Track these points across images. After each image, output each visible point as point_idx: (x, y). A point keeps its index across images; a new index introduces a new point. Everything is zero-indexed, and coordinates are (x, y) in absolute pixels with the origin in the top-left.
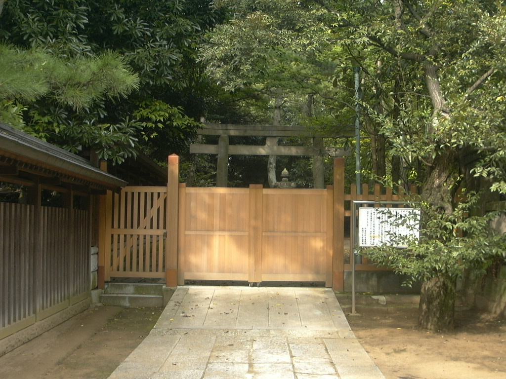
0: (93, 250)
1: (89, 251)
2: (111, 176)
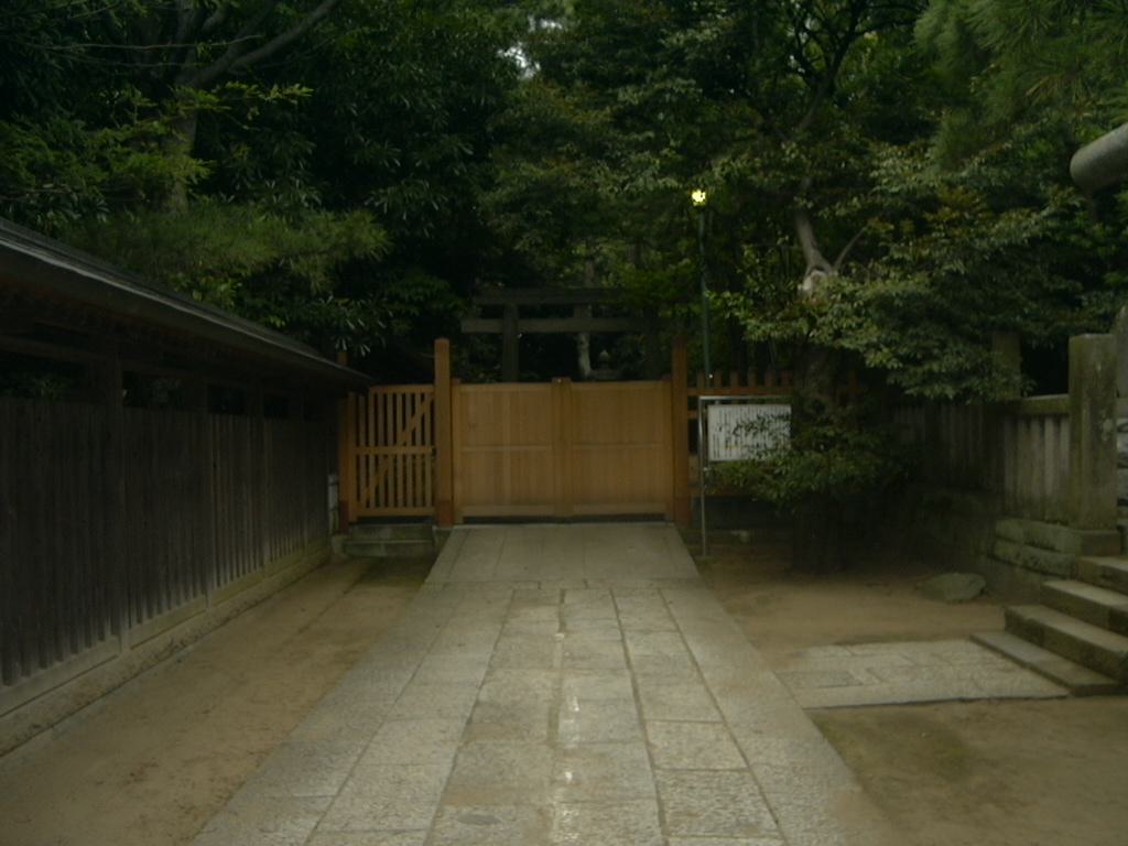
0: (331, 479)
1: (326, 479)
2: (324, 360)
